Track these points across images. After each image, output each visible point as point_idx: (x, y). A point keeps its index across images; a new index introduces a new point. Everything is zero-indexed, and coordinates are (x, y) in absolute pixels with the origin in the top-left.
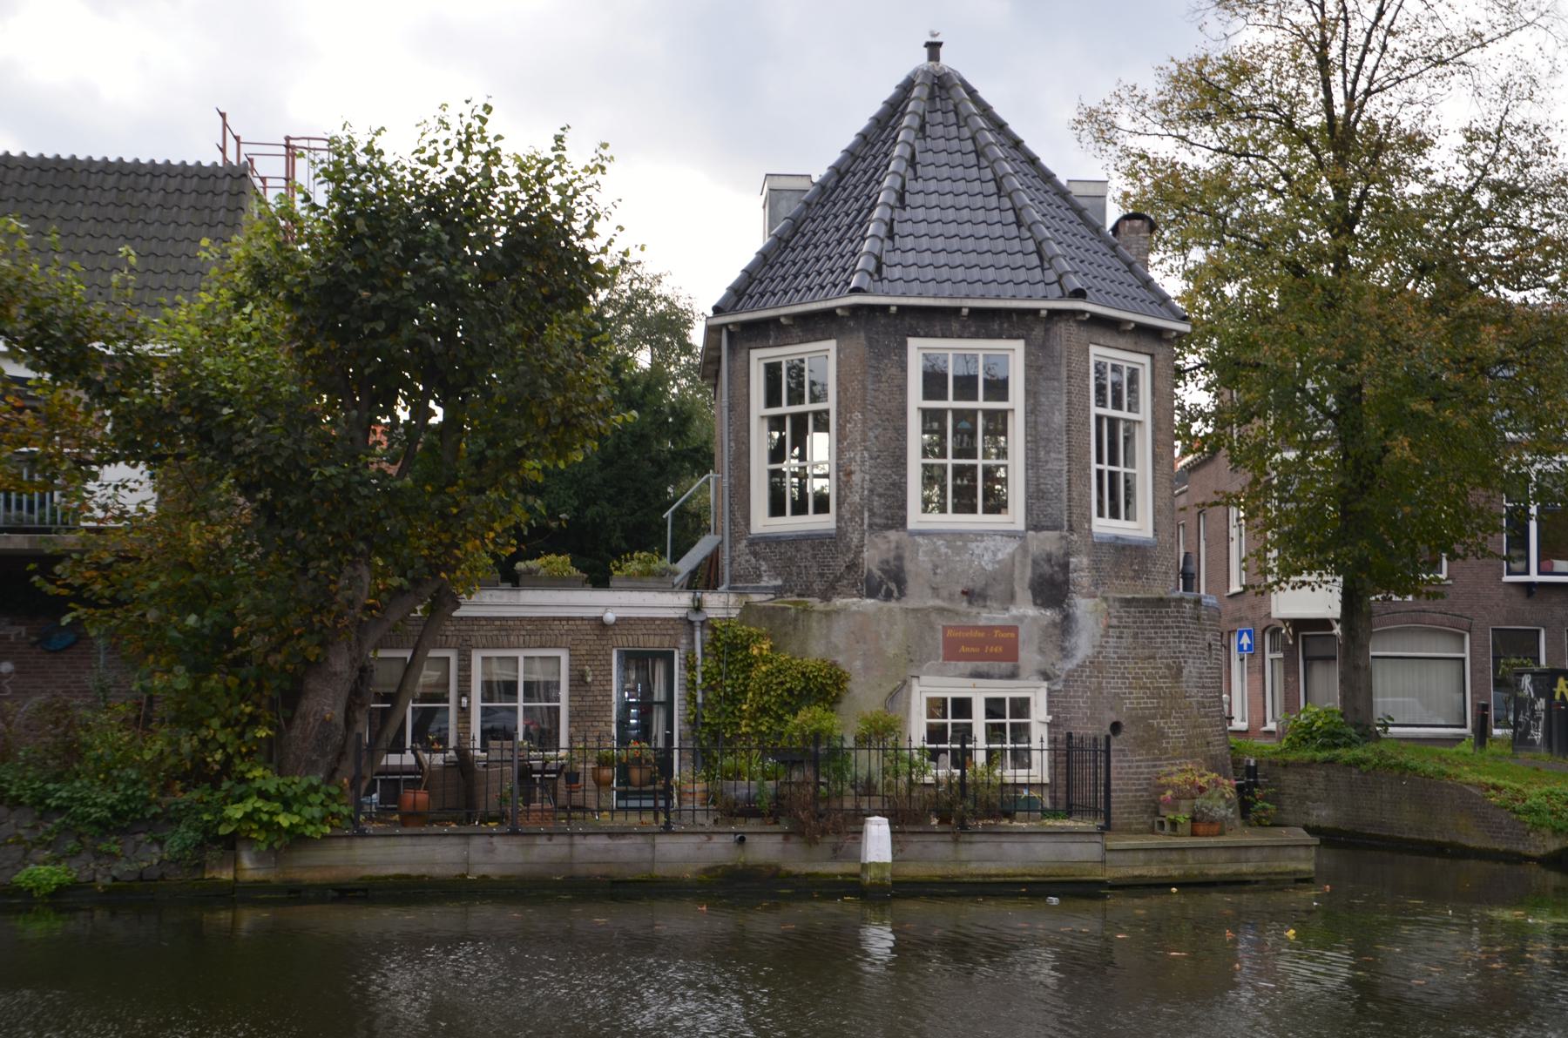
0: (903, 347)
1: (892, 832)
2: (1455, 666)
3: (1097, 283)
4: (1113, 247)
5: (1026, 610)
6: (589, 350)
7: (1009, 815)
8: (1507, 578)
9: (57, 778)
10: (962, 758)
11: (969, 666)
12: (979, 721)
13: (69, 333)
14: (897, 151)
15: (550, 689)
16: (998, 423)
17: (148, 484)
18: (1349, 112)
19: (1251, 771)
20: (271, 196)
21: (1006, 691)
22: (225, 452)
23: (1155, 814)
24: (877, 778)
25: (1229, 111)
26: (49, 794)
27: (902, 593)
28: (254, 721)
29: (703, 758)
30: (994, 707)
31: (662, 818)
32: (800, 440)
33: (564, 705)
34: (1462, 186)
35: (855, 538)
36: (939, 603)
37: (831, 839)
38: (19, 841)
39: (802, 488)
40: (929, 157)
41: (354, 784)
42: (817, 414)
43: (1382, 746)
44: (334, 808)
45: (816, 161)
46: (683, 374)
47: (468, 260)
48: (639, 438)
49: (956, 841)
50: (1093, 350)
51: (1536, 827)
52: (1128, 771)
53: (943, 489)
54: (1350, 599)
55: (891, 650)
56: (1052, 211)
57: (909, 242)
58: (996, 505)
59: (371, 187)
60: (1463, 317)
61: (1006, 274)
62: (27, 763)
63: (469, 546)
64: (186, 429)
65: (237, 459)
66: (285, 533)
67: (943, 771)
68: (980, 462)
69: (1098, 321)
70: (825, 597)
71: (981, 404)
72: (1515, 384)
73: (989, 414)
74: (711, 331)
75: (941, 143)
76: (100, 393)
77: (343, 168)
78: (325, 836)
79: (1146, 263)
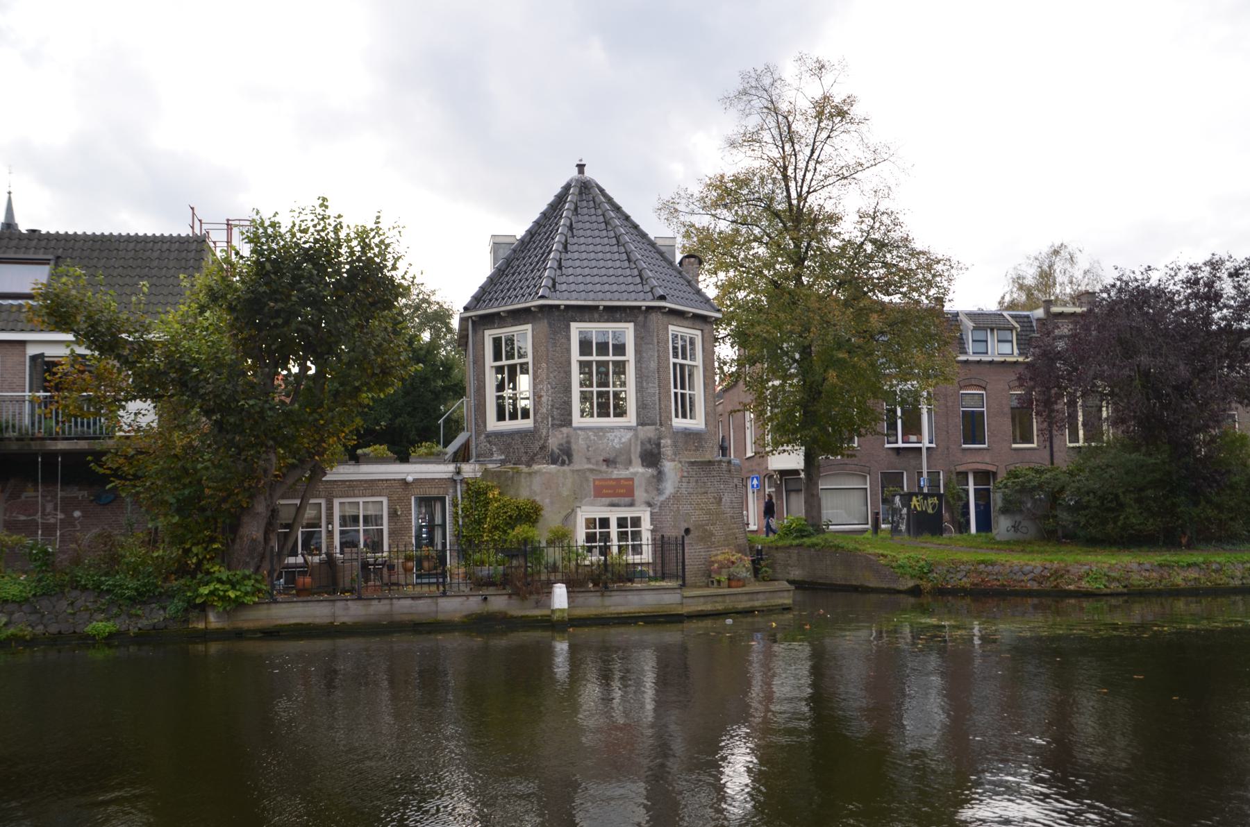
0: (568, 327)
1: (568, 592)
2: (862, 492)
3: (672, 292)
4: (680, 273)
5: (638, 469)
6: (395, 332)
7: (631, 581)
8: (887, 446)
9: (107, 574)
10: (605, 551)
11: (608, 500)
12: (614, 530)
13: (108, 329)
14: (562, 222)
15: (378, 519)
16: (620, 368)
17: (152, 411)
18: (799, 202)
19: (759, 552)
20: (219, 254)
21: (628, 513)
22: (195, 393)
23: (709, 577)
24: (559, 563)
25: (737, 201)
26: (102, 583)
27: (570, 462)
28: (213, 540)
29: (463, 555)
30: (622, 522)
31: (441, 588)
32: (513, 379)
33: (385, 528)
34: (859, 240)
35: (544, 432)
36: (591, 466)
37: (535, 597)
38: (87, 609)
39: (515, 405)
40: (570, 263)
41: (270, 574)
42: (521, 365)
43: (827, 536)
44: (258, 586)
45: (519, 230)
46: (448, 343)
47: (327, 284)
48: (424, 379)
49: (602, 595)
50: (671, 328)
51: (903, 575)
52: (694, 554)
53: (592, 405)
54: (809, 458)
55: (565, 493)
56: (646, 253)
57: (570, 271)
58: (620, 412)
59: (274, 246)
60: (861, 309)
61: (623, 287)
62: (90, 566)
63: (331, 441)
64: (173, 380)
65: (202, 397)
66: (228, 437)
67: (595, 558)
68: (611, 389)
69: (673, 312)
70: (529, 465)
71: (611, 358)
72: (888, 344)
73: (616, 363)
74: (463, 320)
75: (586, 218)
76: (125, 361)
77: (261, 234)
78: (255, 603)
79: (698, 282)
